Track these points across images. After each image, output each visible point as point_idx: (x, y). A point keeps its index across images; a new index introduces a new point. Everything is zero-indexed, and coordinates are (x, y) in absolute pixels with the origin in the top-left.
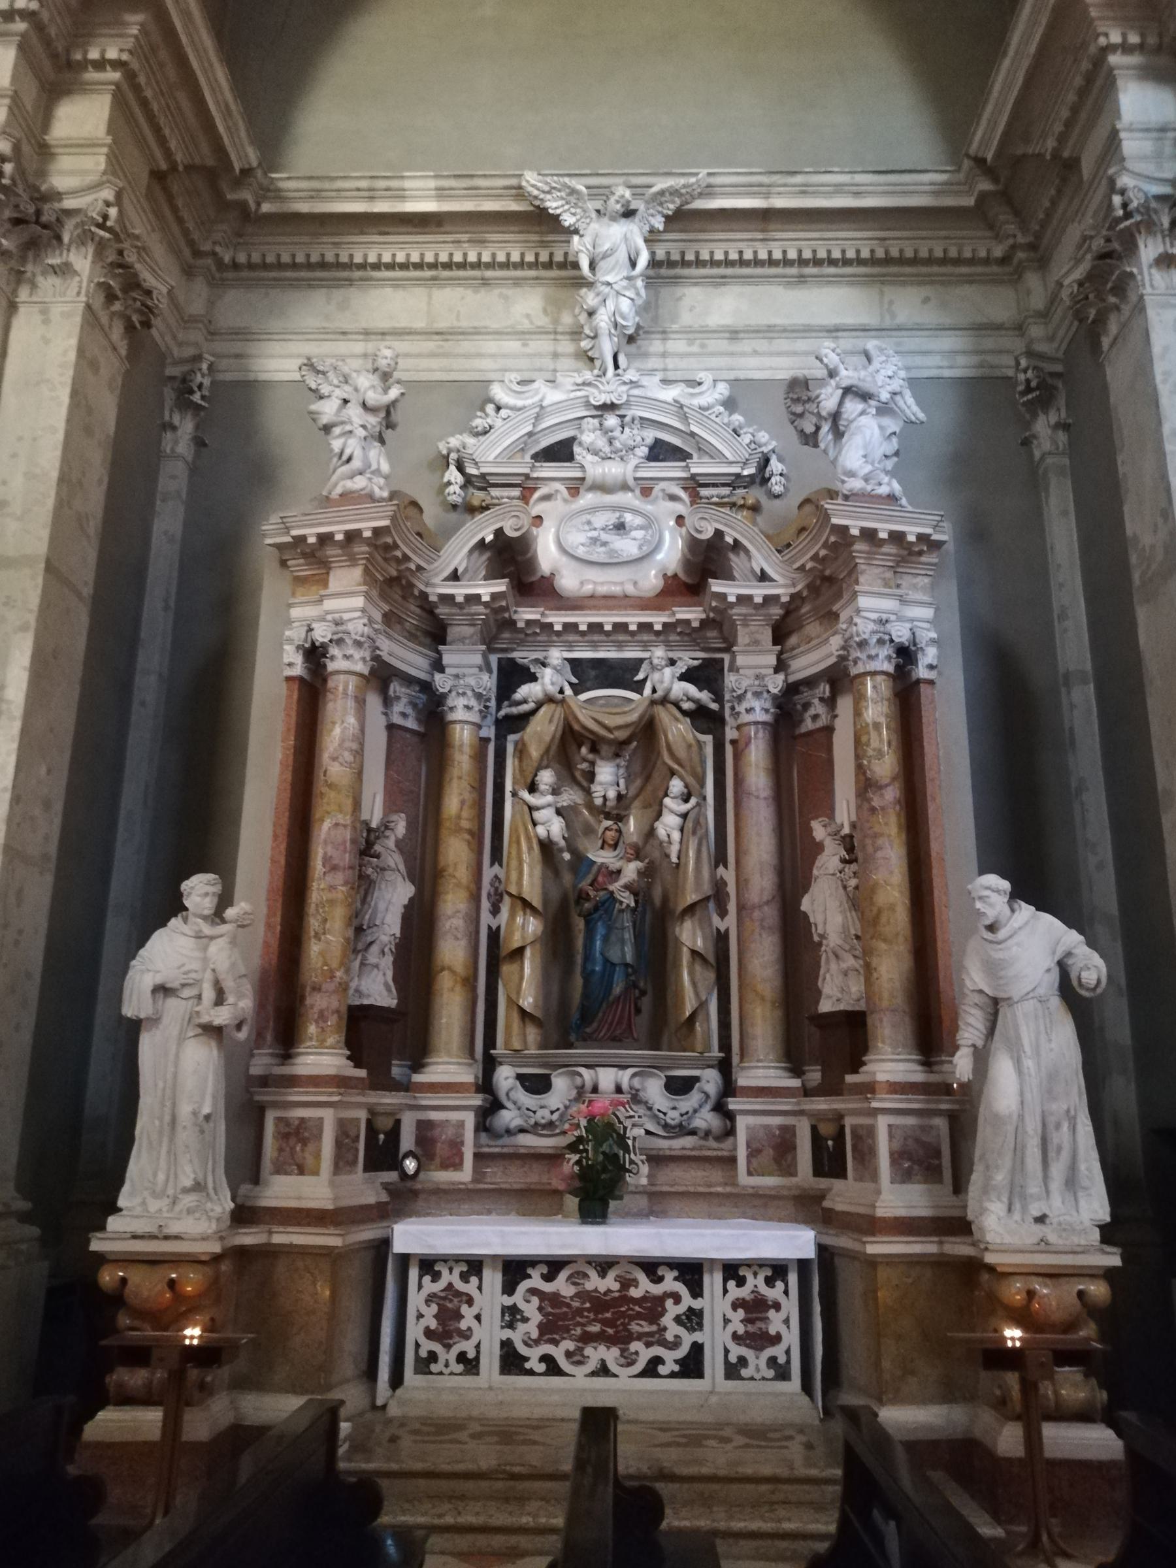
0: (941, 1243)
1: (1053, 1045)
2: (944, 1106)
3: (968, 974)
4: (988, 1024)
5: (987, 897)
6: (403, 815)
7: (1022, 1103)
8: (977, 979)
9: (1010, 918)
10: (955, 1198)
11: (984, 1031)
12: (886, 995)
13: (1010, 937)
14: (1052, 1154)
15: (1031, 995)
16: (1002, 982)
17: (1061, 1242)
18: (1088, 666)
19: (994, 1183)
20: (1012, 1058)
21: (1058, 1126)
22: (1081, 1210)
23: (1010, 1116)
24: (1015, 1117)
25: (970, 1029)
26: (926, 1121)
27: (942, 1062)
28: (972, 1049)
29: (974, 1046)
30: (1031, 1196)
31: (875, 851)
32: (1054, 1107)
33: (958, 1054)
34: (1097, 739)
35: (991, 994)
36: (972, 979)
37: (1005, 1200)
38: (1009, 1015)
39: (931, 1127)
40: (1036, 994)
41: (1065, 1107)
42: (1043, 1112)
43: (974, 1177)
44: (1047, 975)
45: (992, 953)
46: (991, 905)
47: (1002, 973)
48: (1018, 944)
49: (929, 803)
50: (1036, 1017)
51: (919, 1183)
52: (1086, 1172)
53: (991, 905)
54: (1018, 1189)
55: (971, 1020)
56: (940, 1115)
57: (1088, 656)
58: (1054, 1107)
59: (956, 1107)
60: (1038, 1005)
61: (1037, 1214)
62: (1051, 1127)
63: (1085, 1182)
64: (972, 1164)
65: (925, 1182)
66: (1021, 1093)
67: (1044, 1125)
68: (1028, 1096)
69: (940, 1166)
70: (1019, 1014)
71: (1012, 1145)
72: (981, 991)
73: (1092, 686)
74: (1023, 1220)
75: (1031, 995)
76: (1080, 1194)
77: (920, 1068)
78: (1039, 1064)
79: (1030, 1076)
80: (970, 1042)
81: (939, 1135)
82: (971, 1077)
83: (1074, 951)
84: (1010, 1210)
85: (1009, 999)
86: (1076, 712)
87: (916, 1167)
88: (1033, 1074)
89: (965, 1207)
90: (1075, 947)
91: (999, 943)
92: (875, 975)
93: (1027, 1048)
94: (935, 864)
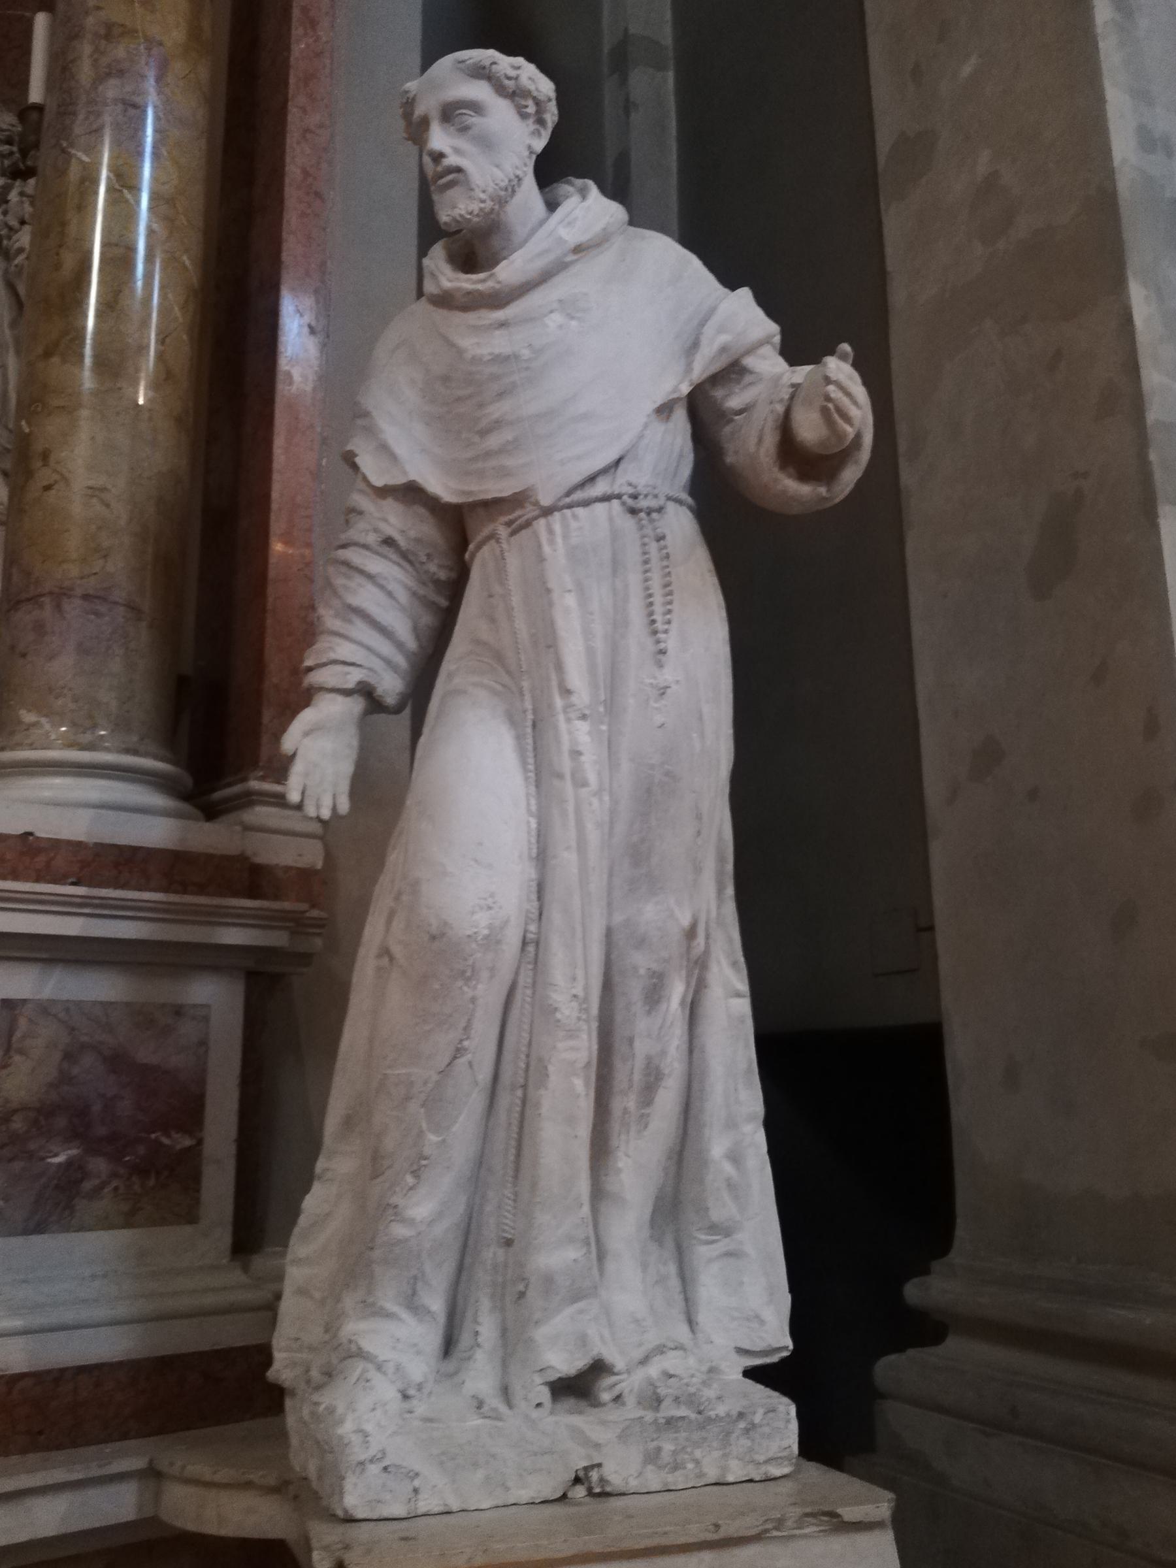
0: (153, 1475)
1: (668, 675)
2: (232, 936)
3: (371, 431)
4: (427, 620)
5: (476, 107)
6: (890, 1495)
7: (541, 889)
8: (401, 448)
9: (542, 223)
10: (236, 1276)
11: (412, 644)
12: (73, 543)
13: (545, 277)
14: (624, 1102)
15: (601, 487)
16: (493, 441)
17: (654, 1479)
18: (666, 36)
19: (399, 1231)
20: (512, 720)
21: (654, 995)
22: (703, 1317)
23: (492, 941)
24: (512, 938)
25: (360, 631)
26: (162, 991)
27: (249, 799)
28: (356, 705)
29: (366, 691)
30: (549, 1280)
31: (100, 78)
32: (650, 913)
33: (306, 717)
34: (674, 181)
35: (448, 497)
36: (384, 448)
37: (437, 1304)
38: (513, 564)
39: (178, 1011)
40: (619, 483)
41: (685, 920)
42: (609, 933)
43: (313, 1203)
44: (659, 429)
45: (468, 343)
46: (486, 143)
47: (496, 410)
48: (569, 308)
49: (297, 31)
50: (616, 565)
51: (105, 1223)
52: (728, 1168)
53: (486, 143)
54: (492, 1254)
55: (366, 597)
56: (215, 969)
57: (668, 15)
58: (650, 913)
59: (277, 939)
60: (628, 524)
61: (565, 1363)
62: (633, 991)
63: (722, 1209)
64: (314, 1146)
65: (128, 1221)
66: (542, 856)
67: (608, 986)
68: (566, 860)
69: (193, 1156)
70: (556, 554)
71: (484, 1074)
72: (411, 493)
73: (670, 75)
74: (505, 1392)
75: (601, 487)
76: (704, 1252)
77: (157, 799)
78: (611, 746)
79: (580, 782)
80: (353, 677)
81: (203, 1043)
82: (344, 806)
83: (749, 362)
84: (449, 1345)
85: (518, 500)
86: (636, 118)
87: (100, 1165)
88: (592, 778)
89: (270, 1309)
90: (751, 350)
91: (497, 300)
92: (44, 476)
93: (576, 677)
94: (293, 196)
